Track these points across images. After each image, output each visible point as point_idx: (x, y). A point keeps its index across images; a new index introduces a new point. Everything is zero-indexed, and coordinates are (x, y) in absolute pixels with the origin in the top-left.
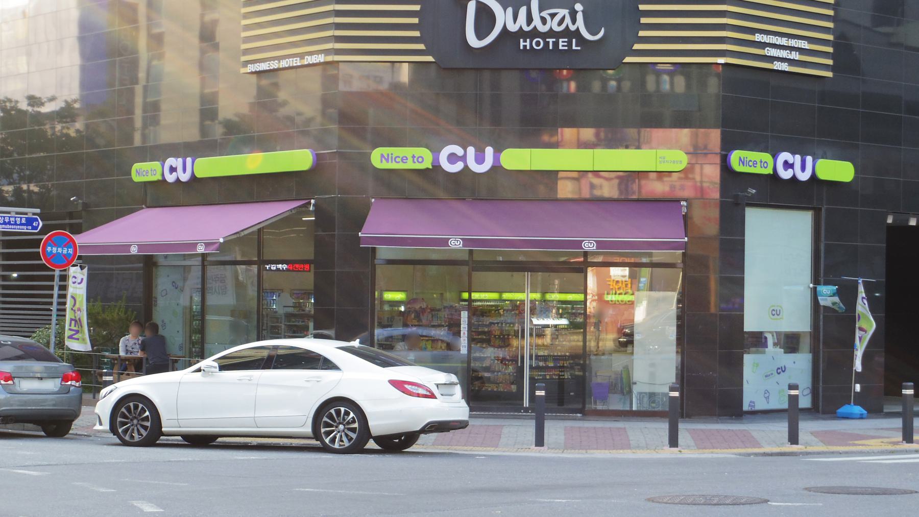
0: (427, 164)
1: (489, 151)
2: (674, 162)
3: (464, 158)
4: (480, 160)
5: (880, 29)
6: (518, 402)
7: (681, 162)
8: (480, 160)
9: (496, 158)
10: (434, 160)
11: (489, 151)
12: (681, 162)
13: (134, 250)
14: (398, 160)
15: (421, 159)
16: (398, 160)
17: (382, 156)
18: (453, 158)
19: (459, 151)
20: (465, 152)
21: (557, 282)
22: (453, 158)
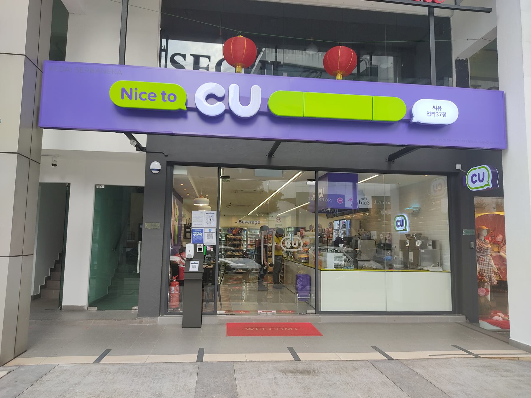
4: (245, 100)
8: (245, 100)
9: (264, 101)
14: (143, 96)
16: (144, 96)
17: (123, 90)
18: (211, 97)
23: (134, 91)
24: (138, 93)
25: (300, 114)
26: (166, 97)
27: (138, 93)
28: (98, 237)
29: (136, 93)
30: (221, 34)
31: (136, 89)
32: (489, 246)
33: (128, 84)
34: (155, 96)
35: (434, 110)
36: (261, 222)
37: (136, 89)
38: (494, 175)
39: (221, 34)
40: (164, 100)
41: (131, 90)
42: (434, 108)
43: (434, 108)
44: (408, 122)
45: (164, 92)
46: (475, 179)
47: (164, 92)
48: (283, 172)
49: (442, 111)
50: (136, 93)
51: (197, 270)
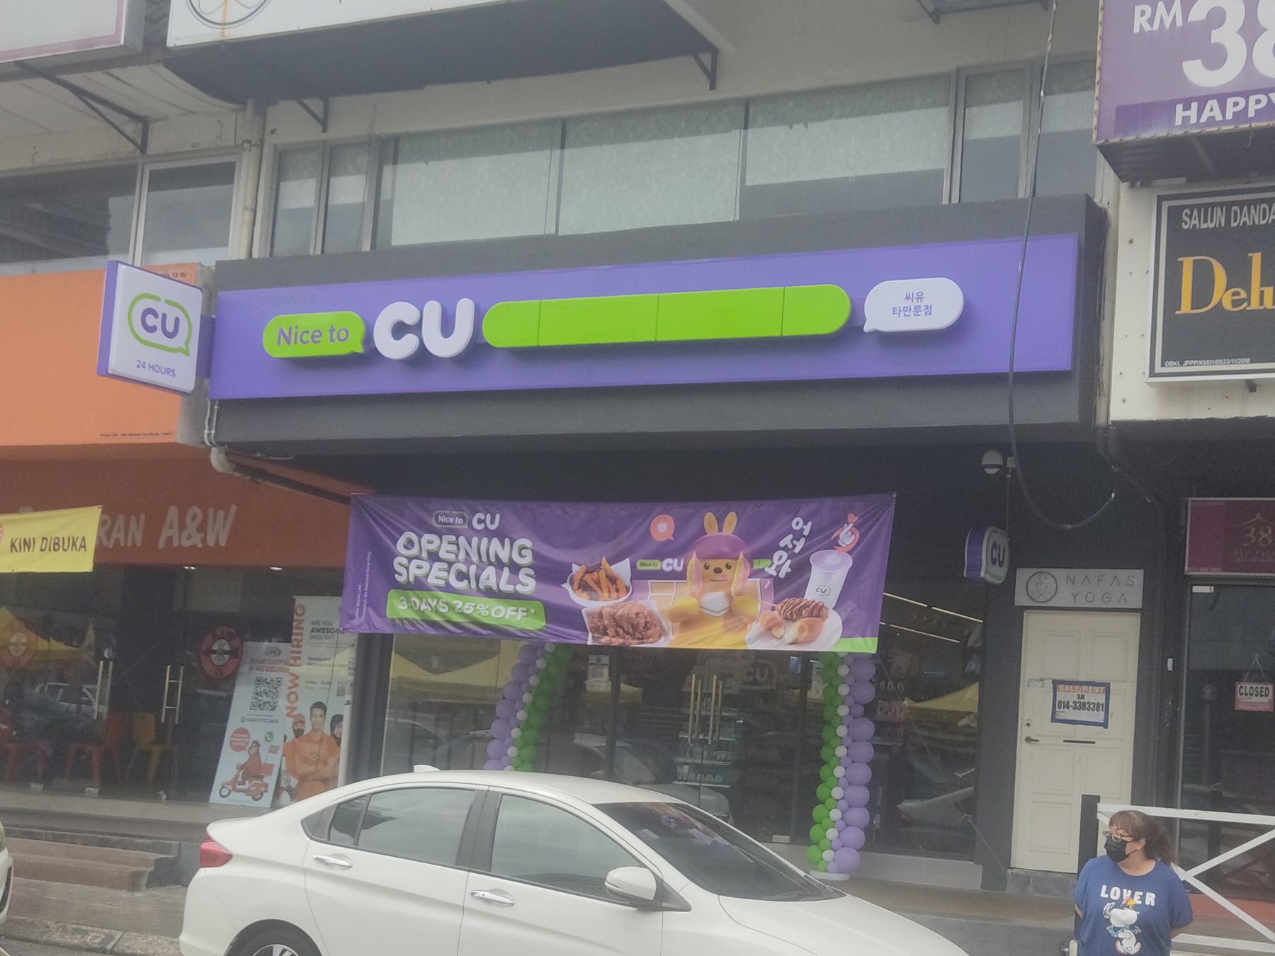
0: (354, 345)
1: (465, 310)
3: (417, 328)
4: (447, 327)
8: (447, 327)
11: (465, 310)
16: (307, 337)
18: (400, 330)
19: (404, 311)
22: (400, 330)
25: (773, 331)
26: (335, 336)
28: (655, 836)
30: (400, 720)
35: (908, 303)
39: (400, 720)
40: (164, 316)
42: (908, 298)
43: (908, 298)
44: (852, 332)
46: (151, 320)
49: (923, 304)
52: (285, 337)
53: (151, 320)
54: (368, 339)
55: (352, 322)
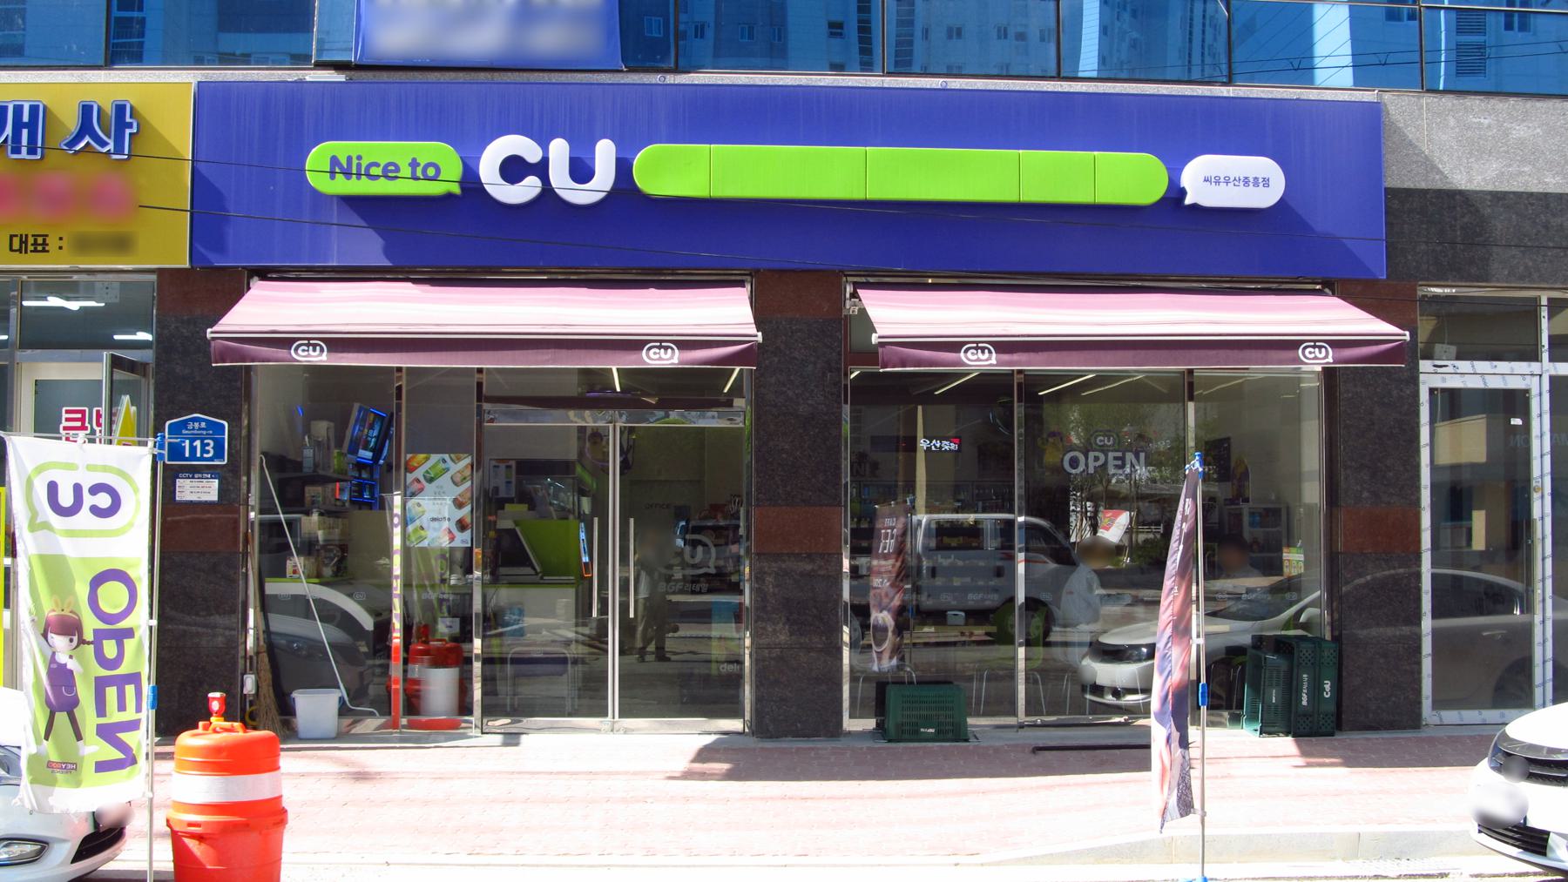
0: (448, 182)
1: (605, 154)
2: (1246, 181)
3: (541, 169)
4: (581, 171)
5: (78, 148)
6: (732, 692)
7: (1266, 182)
8: (581, 171)
9: (624, 168)
10: (1170, 180)
11: (605, 154)
12: (1266, 182)
13: (154, 622)
15: (432, 172)
16: (375, 171)
17: (334, 161)
18: (513, 169)
19: (529, 150)
20: (545, 149)
21: (1304, 703)
23: (355, 162)
24: (364, 163)
27: (364, 163)
29: (359, 166)
31: (359, 158)
32: (876, 582)
33: (342, 149)
34: (397, 169)
36: (1176, 653)
37: (359, 158)
38: (1315, 345)
41: (349, 159)
45: (414, 160)
46: (104, 500)
47: (414, 160)
48: (1470, 181)
50: (359, 166)
51: (215, 498)
52: (336, 167)
53: (104, 500)
54: (470, 180)
55: (445, 158)
